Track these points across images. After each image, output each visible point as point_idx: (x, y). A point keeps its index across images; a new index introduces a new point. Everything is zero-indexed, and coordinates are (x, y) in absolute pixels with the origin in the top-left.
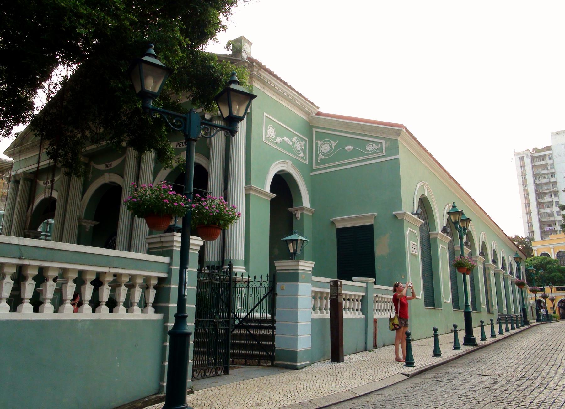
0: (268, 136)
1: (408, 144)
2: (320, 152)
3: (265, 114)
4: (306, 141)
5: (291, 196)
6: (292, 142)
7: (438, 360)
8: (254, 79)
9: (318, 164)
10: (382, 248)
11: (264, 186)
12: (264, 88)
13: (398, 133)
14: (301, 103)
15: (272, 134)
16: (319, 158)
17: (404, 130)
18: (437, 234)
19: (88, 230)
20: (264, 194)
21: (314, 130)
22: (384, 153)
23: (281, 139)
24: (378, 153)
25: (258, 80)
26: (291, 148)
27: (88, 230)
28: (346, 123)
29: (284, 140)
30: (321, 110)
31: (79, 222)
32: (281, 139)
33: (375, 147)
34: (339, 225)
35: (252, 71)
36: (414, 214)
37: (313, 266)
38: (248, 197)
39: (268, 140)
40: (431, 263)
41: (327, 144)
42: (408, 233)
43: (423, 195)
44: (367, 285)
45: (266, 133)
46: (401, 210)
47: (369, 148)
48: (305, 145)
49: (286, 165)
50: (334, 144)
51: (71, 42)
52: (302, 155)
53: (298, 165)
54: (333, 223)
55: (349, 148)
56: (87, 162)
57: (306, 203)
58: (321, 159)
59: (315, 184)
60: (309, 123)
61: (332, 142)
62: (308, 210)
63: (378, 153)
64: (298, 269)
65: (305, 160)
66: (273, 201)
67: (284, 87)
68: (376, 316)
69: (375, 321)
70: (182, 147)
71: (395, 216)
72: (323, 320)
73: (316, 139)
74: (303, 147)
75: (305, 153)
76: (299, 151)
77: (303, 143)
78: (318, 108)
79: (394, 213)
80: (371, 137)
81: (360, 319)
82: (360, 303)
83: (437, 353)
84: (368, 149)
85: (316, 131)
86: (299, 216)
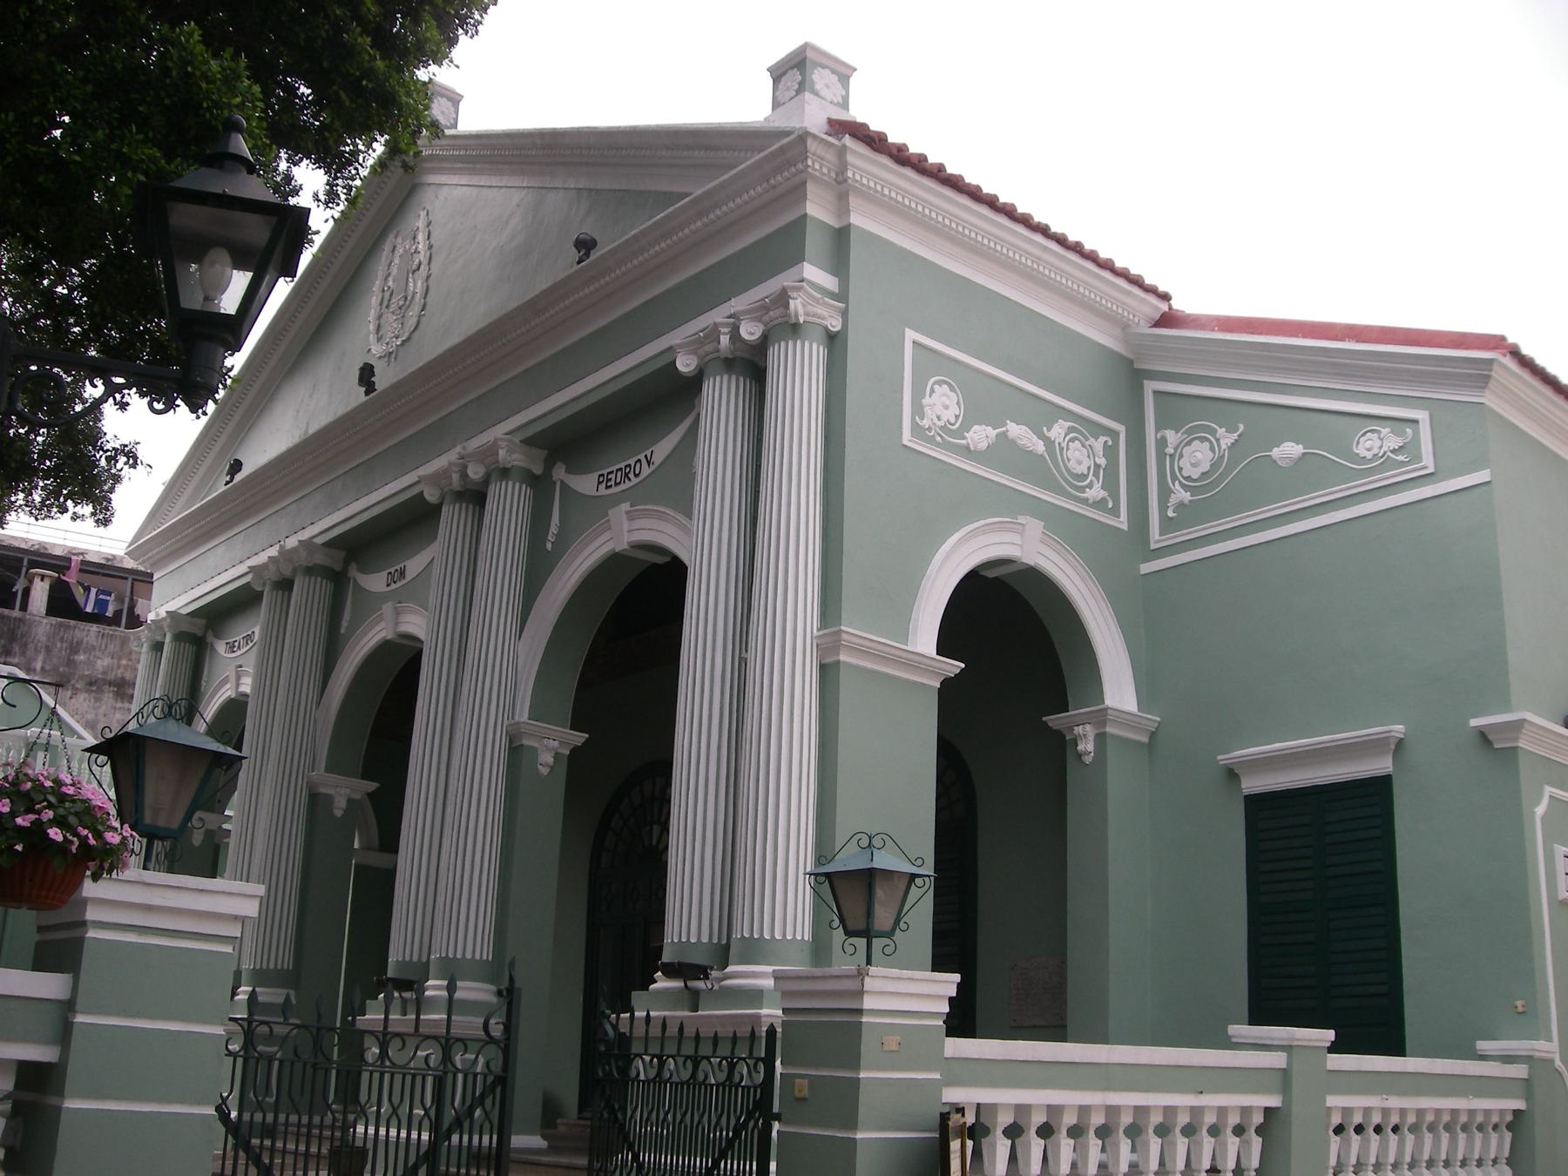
0: (926, 423)
3: (911, 335)
4: (1114, 434)
6: (1049, 443)
9: (1167, 525)
15: (949, 415)
16: (1173, 500)
17: (1508, 362)
19: (544, 771)
20: (914, 662)
21: (1150, 386)
22: (1428, 462)
23: (992, 433)
24: (1403, 464)
29: (1004, 434)
32: (992, 433)
34: (1254, 784)
39: (931, 440)
41: (1203, 439)
42: (1540, 810)
45: (918, 409)
47: (1368, 445)
48: (1110, 452)
49: (1016, 538)
50: (1227, 439)
51: (60, 125)
52: (1096, 492)
53: (1061, 525)
54: (1232, 775)
55: (1289, 450)
56: (338, 568)
57: (1119, 690)
58: (1180, 506)
59: (1151, 610)
60: (1131, 362)
61: (1221, 431)
62: (1124, 718)
63: (1403, 464)
65: (1115, 512)
66: (948, 689)
73: (1159, 427)
74: (1102, 461)
75: (1111, 484)
76: (1083, 477)
77: (1099, 444)
78: (1165, 297)
79: (1474, 722)
82: (1508, 1136)
85: (1156, 393)
86: (1090, 747)
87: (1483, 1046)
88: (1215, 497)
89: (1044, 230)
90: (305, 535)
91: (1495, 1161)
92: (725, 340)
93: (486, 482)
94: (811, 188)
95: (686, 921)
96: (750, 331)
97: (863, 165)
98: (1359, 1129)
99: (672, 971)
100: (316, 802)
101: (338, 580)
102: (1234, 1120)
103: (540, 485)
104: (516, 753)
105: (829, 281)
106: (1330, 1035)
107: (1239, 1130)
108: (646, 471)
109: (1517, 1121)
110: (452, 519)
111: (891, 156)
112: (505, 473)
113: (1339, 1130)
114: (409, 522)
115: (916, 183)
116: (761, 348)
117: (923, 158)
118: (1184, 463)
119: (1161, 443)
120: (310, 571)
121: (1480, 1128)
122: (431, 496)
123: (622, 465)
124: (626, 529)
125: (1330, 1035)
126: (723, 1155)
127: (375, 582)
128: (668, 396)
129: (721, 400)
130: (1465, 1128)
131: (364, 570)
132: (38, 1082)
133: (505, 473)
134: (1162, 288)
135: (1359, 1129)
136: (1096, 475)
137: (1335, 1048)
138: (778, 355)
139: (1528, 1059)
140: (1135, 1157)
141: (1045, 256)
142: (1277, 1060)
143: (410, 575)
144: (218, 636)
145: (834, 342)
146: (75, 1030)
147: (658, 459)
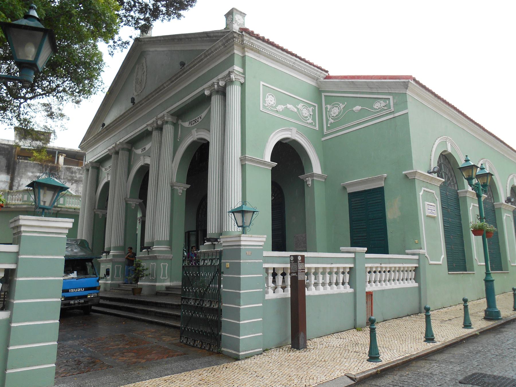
0: (266, 105)
1: (417, 94)
2: (330, 117)
5: (301, 163)
6: (298, 109)
7: (430, 346)
8: (246, 49)
9: (328, 128)
10: (392, 212)
11: (263, 155)
12: (259, 57)
13: (406, 85)
14: (305, 68)
15: (272, 103)
16: (329, 122)
17: (412, 82)
18: (467, 192)
19: (133, 208)
21: (323, 94)
22: (392, 109)
24: (386, 109)
25: (252, 50)
26: (297, 115)
27: (133, 208)
28: (352, 81)
30: (331, 74)
31: (126, 201)
33: (383, 104)
34: (351, 190)
35: (243, 41)
36: (430, 173)
37: (264, 239)
38: (243, 167)
39: (268, 109)
40: (461, 224)
41: (336, 107)
42: (421, 193)
43: (445, 151)
44: (355, 255)
45: (264, 101)
46: (413, 169)
47: (377, 105)
48: (314, 111)
49: (290, 133)
50: (342, 106)
52: (310, 121)
53: (303, 131)
54: (344, 188)
55: (358, 108)
56: (130, 148)
57: (317, 168)
58: (331, 123)
59: (326, 150)
61: (341, 104)
62: (318, 176)
63: (386, 109)
64: (240, 245)
65: (315, 126)
66: (274, 170)
67: (282, 54)
68: (369, 288)
69: (369, 295)
70: (193, 125)
71: (406, 176)
72: (284, 300)
74: (312, 113)
75: (314, 119)
77: (311, 109)
78: (327, 72)
79: (404, 173)
80: (378, 93)
81: (347, 294)
83: (467, 325)
84: (376, 107)
86: (310, 183)
87: (407, 251)
88: (338, 121)
89: (296, 56)
90: (121, 141)
91: (410, 279)
92: (216, 86)
93: (163, 124)
94: (235, 47)
95: (212, 229)
96: (222, 83)
97: (247, 38)
98: (375, 272)
99: (209, 240)
100: (95, 215)
101: (130, 151)
102: (341, 270)
103: (175, 125)
104: (173, 190)
105: (241, 70)
106: (366, 249)
107: (343, 273)
108: (200, 120)
109: (416, 269)
110: (155, 133)
111: (255, 37)
112: (167, 122)
113: (369, 272)
114: (146, 135)
115: (262, 44)
116: (224, 88)
117: (263, 38)
118: (332, 113)
119: (326, 108)
120: (123, 149)
121: (406, 271)
122: (150, 129)
123: (159, 116)
124: (195, 135)
125: (366, 249)
126: (211, 283)
127: (139, 151)
128: (203, 101)
129: (216, 100)
130: (402, 271)
131: (136, 149)
132: (10, 274)
133: (167, 122)
134: (326, 70)
135: (375, 272)
136: (310, 117)
137: (367, 252)
138: (228, 89)
139: (418, 254)
140: (323, 281)
141: (301, 64)
142: (352, 255)
143: (147, 149)
144: (103, 167)
145: (243, 85)
146: (19, 260)
147: (202, 117)
